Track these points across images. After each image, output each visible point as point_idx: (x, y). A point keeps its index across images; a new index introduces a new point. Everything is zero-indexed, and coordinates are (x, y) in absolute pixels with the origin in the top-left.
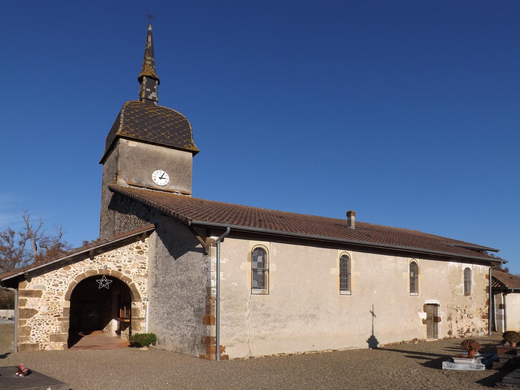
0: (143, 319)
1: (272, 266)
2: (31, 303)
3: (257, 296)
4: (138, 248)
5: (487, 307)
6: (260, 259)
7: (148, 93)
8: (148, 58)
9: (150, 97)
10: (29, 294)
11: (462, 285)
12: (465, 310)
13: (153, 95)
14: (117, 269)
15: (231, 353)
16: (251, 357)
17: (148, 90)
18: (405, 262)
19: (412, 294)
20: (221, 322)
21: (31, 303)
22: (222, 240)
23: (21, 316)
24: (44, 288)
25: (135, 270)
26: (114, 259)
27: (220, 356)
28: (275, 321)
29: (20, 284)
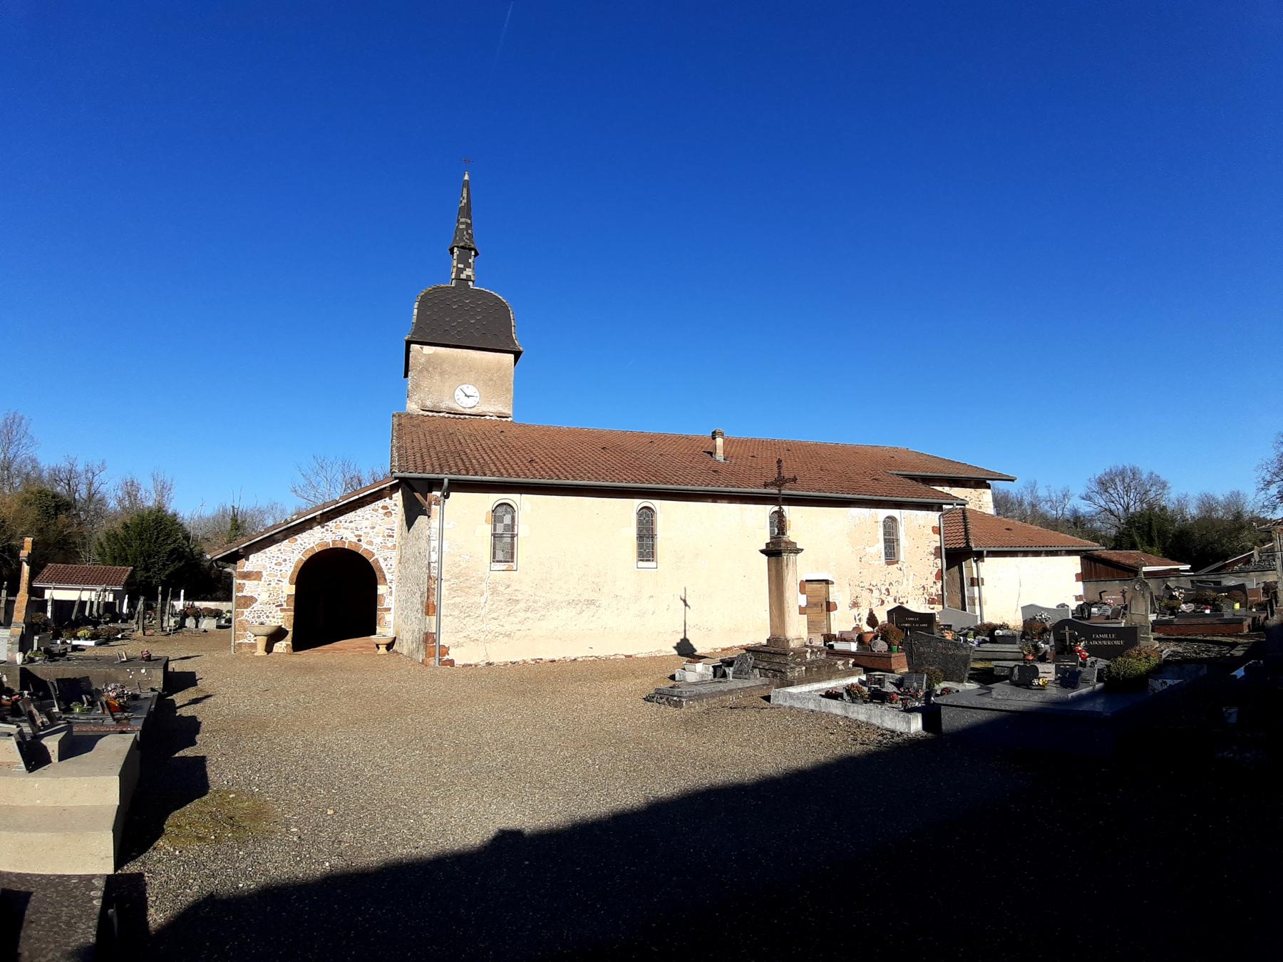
0: (389, 609)
1: (522, 529)
2: (250, 588)
3: (498, 573)
4: (385, 508)
5: (939, 585)
6: (507, 519)
7: (460, 271)
8: (462, 220)
9: (463, 276)
10: (247, 576)
11: (881, 545)
12: (888, 590)
13: (469, 272)
14: (355, 540)
15: (459, 656)
16: (489, 664)
17: (461, 266)
18: (767, 510)
19: (641, 564)
20: (443, 611)
21: (250, 588)
22: (447, 497)
23: (238, 606)
24: (265, 567)
25: (380, 539)
26: (352, 525)
27: (712, 682)
28: (526, 610)
29: (239, 563)
